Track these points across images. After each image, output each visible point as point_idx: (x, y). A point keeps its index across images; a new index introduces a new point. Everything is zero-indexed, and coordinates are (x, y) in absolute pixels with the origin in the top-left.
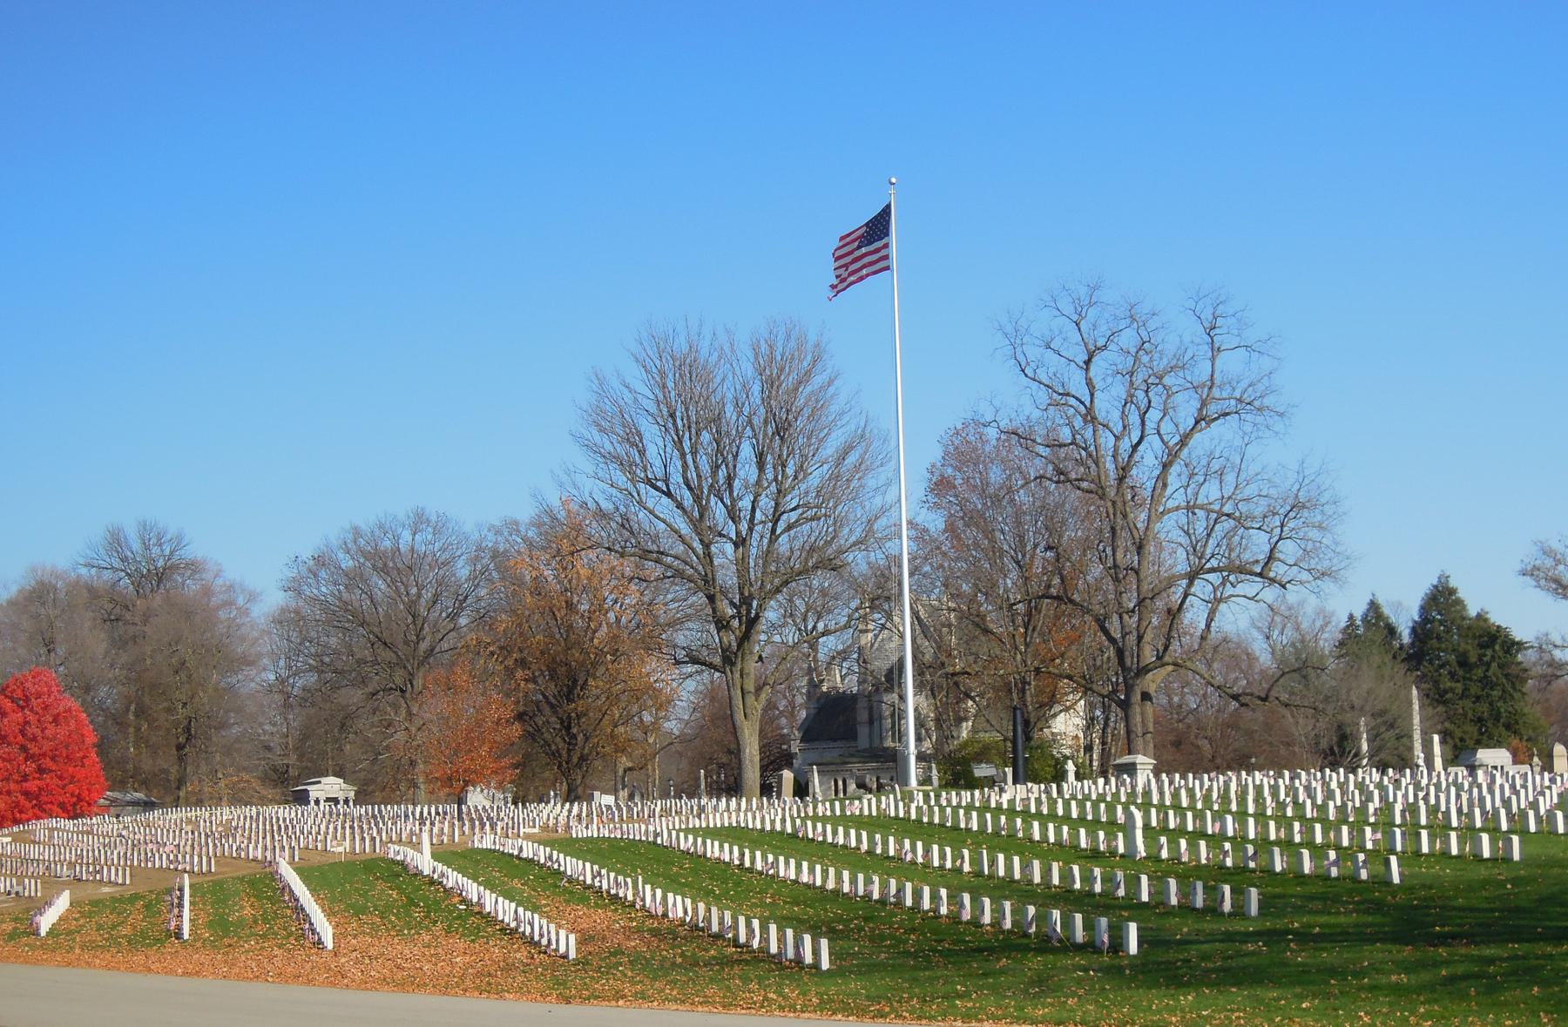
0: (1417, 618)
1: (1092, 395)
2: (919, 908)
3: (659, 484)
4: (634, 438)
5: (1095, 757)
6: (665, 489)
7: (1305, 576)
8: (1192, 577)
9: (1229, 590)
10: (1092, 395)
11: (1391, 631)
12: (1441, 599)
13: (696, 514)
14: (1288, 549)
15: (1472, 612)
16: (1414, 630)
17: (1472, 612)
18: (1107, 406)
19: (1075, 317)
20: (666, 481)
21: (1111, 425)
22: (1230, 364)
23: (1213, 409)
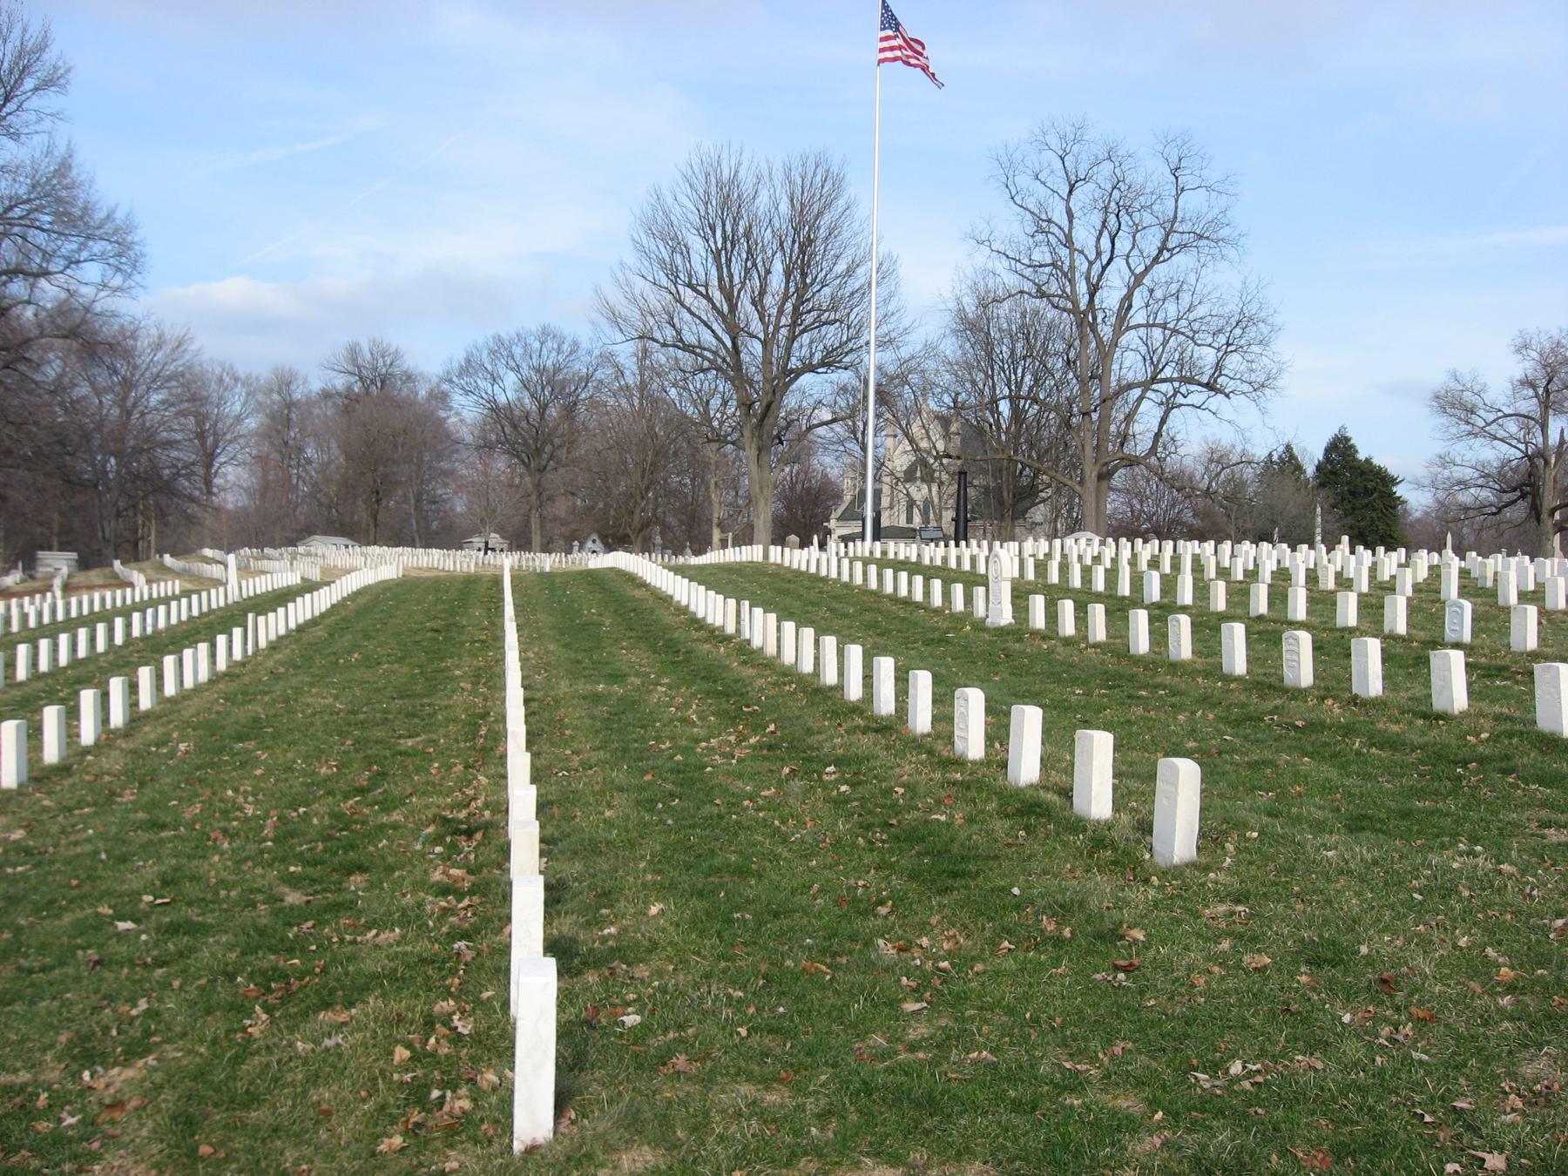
0: (1321, 458)
1: (1071, 222)
2: (1086, 638)
3: (700, 288)
4: (679, 247)
5: (1127, 568)
6: (704, 292)
7: (1246, 388)
8: (1147, 385)
9: (1179, 399)
10: (1071, 222)
11: (1299, 468)
12: (1340, 448)
13: (726, 309)
14: (1234, 362)
15: (1362, 456)
16: (1319, 468)
17: (1362, 456)
18: (1084, 236)
19: (1060, 153)
20: (706, 286)
21: (1086, 252)
22: (1192, 203)
23: (1174, 241)
